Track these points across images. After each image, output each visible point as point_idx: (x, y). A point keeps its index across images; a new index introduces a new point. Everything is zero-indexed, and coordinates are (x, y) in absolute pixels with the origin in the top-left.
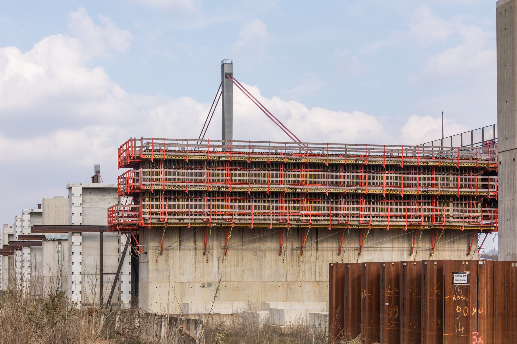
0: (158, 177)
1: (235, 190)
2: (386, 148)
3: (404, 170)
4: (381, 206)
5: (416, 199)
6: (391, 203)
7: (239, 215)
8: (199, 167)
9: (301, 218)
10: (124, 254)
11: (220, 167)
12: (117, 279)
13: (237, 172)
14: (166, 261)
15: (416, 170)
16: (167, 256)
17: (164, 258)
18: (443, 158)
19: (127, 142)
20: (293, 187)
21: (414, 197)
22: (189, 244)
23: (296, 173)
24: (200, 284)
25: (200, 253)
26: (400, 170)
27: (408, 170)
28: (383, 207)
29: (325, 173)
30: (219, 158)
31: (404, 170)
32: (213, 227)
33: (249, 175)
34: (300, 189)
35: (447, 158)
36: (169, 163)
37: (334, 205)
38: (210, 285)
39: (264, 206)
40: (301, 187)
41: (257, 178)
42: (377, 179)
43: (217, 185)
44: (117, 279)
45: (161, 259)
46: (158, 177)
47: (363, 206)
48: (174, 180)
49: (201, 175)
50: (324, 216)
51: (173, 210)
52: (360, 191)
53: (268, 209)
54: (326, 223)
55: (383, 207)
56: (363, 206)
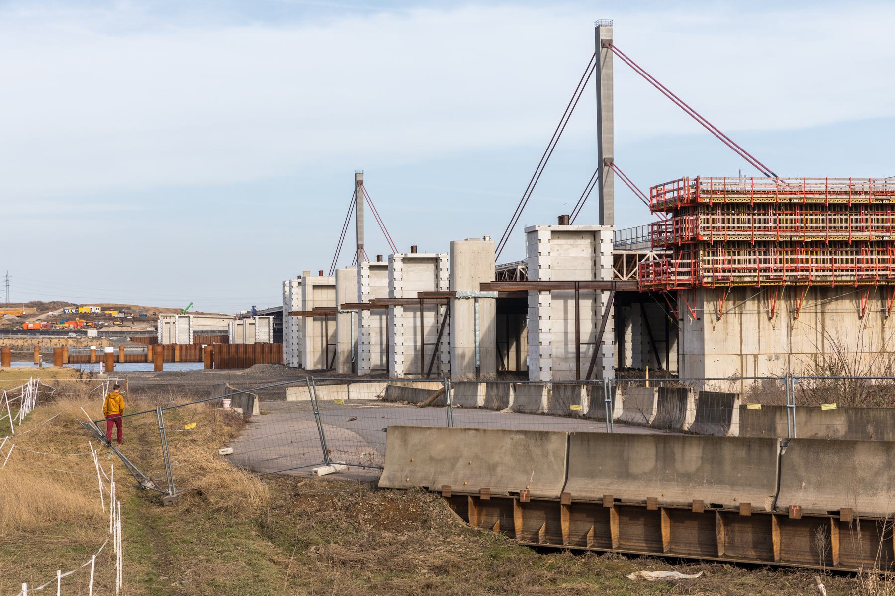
0: (767, 225)
1: (810, 240)
2: (806, 182)
3: (851, 209)
4: (822, 257)
5: (802, 247)
6: (817, 252)
7: (817, 271)
8: (762, 211)
9: (888, 272)
10: (605, 318)
11: (789, 212)
12: (436, 349)
13: (809, 217)
14: (725, 328)
15: (866, 210)
16: (726, 322)
17: (722, 325)
18: (856, 193)
19: (674, 182)
20: (880, 234)
21: (864, 243)
22: (751, 306)
23: (880, 217)
24: (766, 357)
25: (764, 317)
26: (846, 210)
27: (856, 209)
28: (825, 257)
29: (750, 217)
30: (790, 199)
31: (851, 209)
32: (787, 286)
33: (841, 219)
34: (889, 237)
35: (859, 193)
36: (728, 207)
37: (762, 257)
38: (777, 356)
39: (842, 259)
40: (888, 234)
41: (833, 225)
42: (841, 219)
43: (789, 234)
44: (436, 349)
45: (719, 325)
46: (767, 225)
47: (800, 257)
48: (734, 228)
49: (765, 221)
50: (750, 271)
51: (806, 265)
52: (796, 239)
53: (755, 262)
54: (848, 278)
55: (825, 257)
56: (800, 257)
